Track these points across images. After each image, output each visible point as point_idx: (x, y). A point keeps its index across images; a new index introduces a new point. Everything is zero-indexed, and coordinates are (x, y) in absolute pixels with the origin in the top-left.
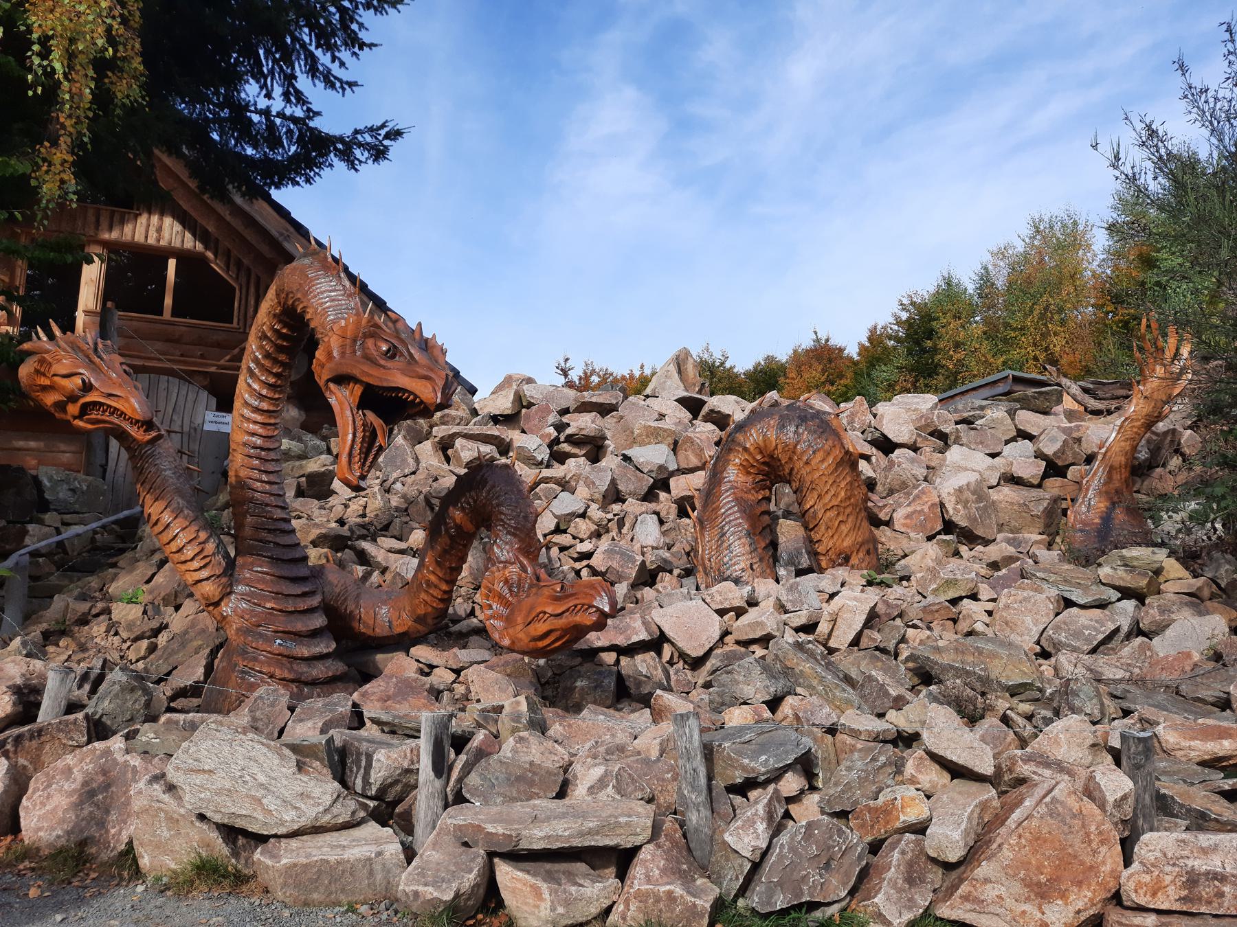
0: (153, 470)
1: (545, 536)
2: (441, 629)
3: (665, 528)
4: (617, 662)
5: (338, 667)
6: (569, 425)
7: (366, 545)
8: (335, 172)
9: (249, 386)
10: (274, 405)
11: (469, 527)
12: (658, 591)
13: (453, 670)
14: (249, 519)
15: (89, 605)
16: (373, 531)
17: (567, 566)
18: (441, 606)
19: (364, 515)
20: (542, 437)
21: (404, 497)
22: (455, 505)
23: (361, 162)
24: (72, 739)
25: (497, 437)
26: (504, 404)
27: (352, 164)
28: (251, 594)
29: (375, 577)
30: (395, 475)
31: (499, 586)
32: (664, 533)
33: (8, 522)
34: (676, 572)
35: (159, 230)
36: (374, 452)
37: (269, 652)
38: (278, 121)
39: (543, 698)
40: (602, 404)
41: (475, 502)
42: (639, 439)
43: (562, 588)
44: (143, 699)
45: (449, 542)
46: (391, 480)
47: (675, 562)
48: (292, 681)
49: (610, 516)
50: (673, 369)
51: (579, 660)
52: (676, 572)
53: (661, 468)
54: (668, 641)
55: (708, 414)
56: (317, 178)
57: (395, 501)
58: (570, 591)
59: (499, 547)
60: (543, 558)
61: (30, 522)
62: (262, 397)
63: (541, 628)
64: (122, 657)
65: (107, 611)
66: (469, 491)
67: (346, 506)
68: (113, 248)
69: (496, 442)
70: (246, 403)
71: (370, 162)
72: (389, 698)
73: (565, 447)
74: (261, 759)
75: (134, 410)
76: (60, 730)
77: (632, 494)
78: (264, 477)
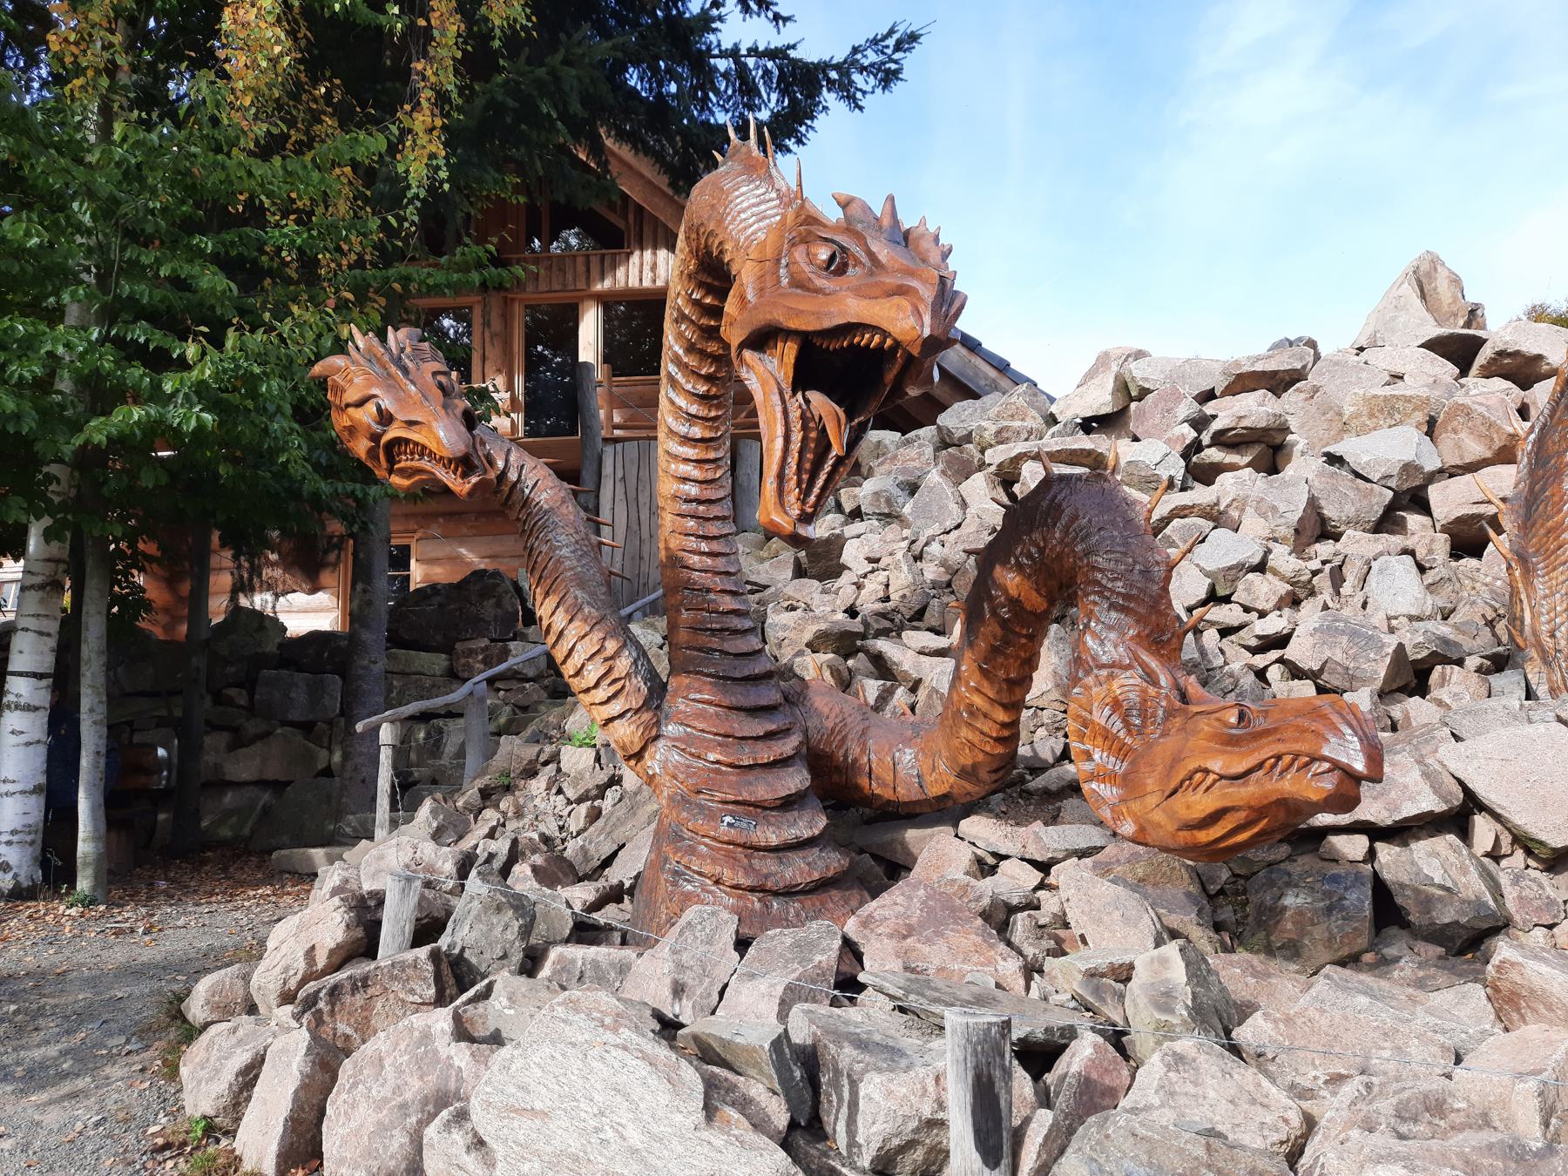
0: (545, 548)
1: (1190, 610)
2: (1012, 784)
3: (1430, 577)
4: (1371, 854)
5: (831, 861)
6: (1214, 417)
7: (883, 645)
8: (833, 119)
9: (672, 402)
10: (711, 428)
11: (1036, 601)
12: (1440, 703)
13: (1033, 863)
14: (685, 615)
15: (537, 748)
16: (893, 623)
17: (1238, 661)
18: (999, 750)
19: (887, 599)
20: (1168, 442)
21: (944, 563)
22: (1005, 563)
23: (864, 93)
24: (412, 992)
25: (1090, 453)
26: (1100, 400)
27: (850, 97)
28: (687, 739)
29: (901, 696)
30: (929, 532)
31: (1100, 716)
32: (1431, 588)
33: (492, 641)
34: (1472, 662)
35: (654, 268)
36: (827, 468)
37: (714, 839)
38: (751, 62)
39: (1218, 927)
40: (1275, 373)
41: (1041, 551)
42: (1354, 423)
43: (1241, 716)
44: (516, 925)
45: (999, 631)
46: (922, 540)
47: (1467, 643)
48: (752, 890)
49: (1315, 565)
50: (1410, 293)
51: (1285, 849)
52: (1472, 662)
53: (1408, 468)
54: (1483, 808)
55: (1492, 361)
56: (811, 134)
57: (931, 572)
58: (1261, 724)
59: (1095, 635)
60: (1189, 650)
61: (514, 639)
62: (692, 418)
63: (1201, 803)
64: (561, 828)
65: (555, 758)
66: (1029, 533)
67: (859, 586)
68: (608, 302)
69: (1089, 460)
70: (671, 431)
71: (879, 91)
72: (909, 931)
73: (1213, 455)
74: (637, 1091)
75: (439, 441)
76: (394, 978)
77: (1353, 522)
78: (704, 547)
